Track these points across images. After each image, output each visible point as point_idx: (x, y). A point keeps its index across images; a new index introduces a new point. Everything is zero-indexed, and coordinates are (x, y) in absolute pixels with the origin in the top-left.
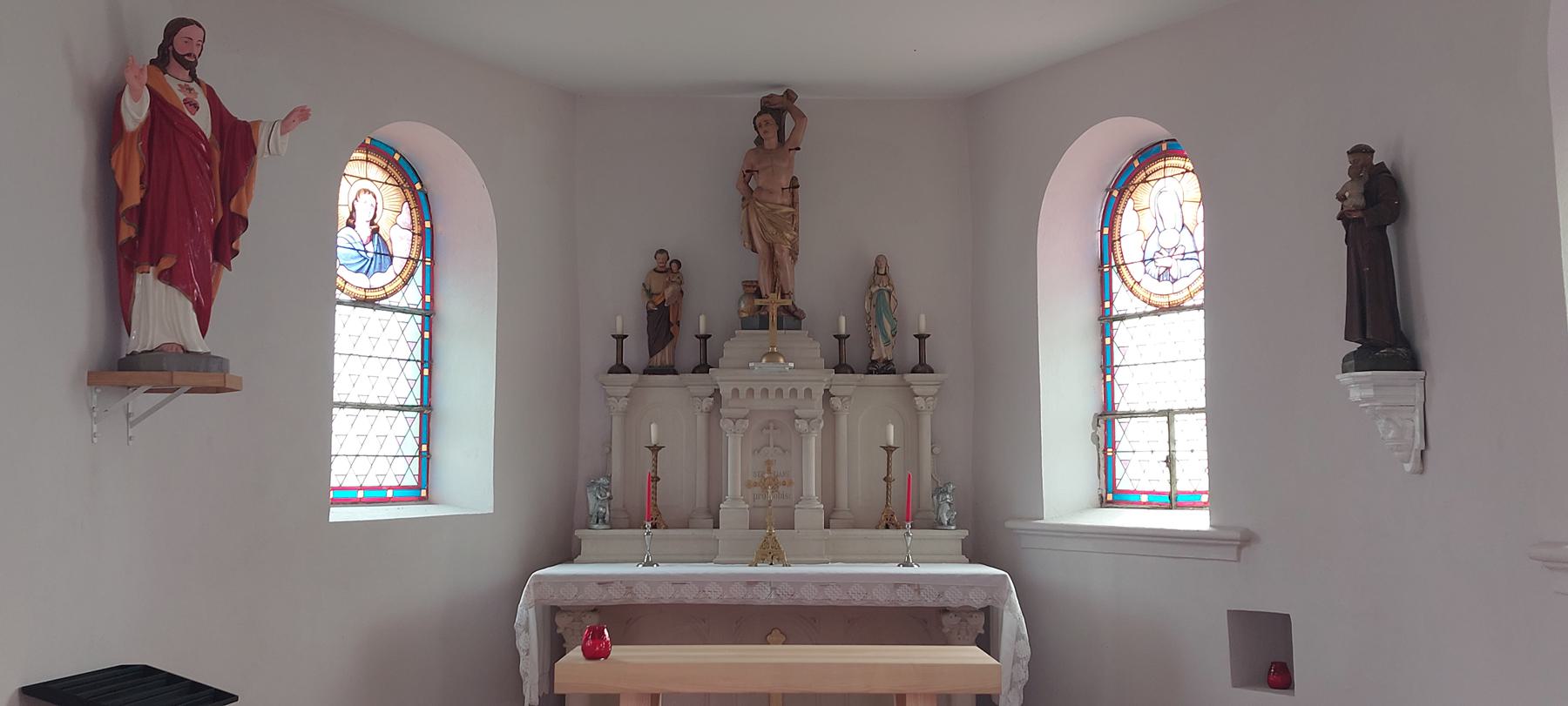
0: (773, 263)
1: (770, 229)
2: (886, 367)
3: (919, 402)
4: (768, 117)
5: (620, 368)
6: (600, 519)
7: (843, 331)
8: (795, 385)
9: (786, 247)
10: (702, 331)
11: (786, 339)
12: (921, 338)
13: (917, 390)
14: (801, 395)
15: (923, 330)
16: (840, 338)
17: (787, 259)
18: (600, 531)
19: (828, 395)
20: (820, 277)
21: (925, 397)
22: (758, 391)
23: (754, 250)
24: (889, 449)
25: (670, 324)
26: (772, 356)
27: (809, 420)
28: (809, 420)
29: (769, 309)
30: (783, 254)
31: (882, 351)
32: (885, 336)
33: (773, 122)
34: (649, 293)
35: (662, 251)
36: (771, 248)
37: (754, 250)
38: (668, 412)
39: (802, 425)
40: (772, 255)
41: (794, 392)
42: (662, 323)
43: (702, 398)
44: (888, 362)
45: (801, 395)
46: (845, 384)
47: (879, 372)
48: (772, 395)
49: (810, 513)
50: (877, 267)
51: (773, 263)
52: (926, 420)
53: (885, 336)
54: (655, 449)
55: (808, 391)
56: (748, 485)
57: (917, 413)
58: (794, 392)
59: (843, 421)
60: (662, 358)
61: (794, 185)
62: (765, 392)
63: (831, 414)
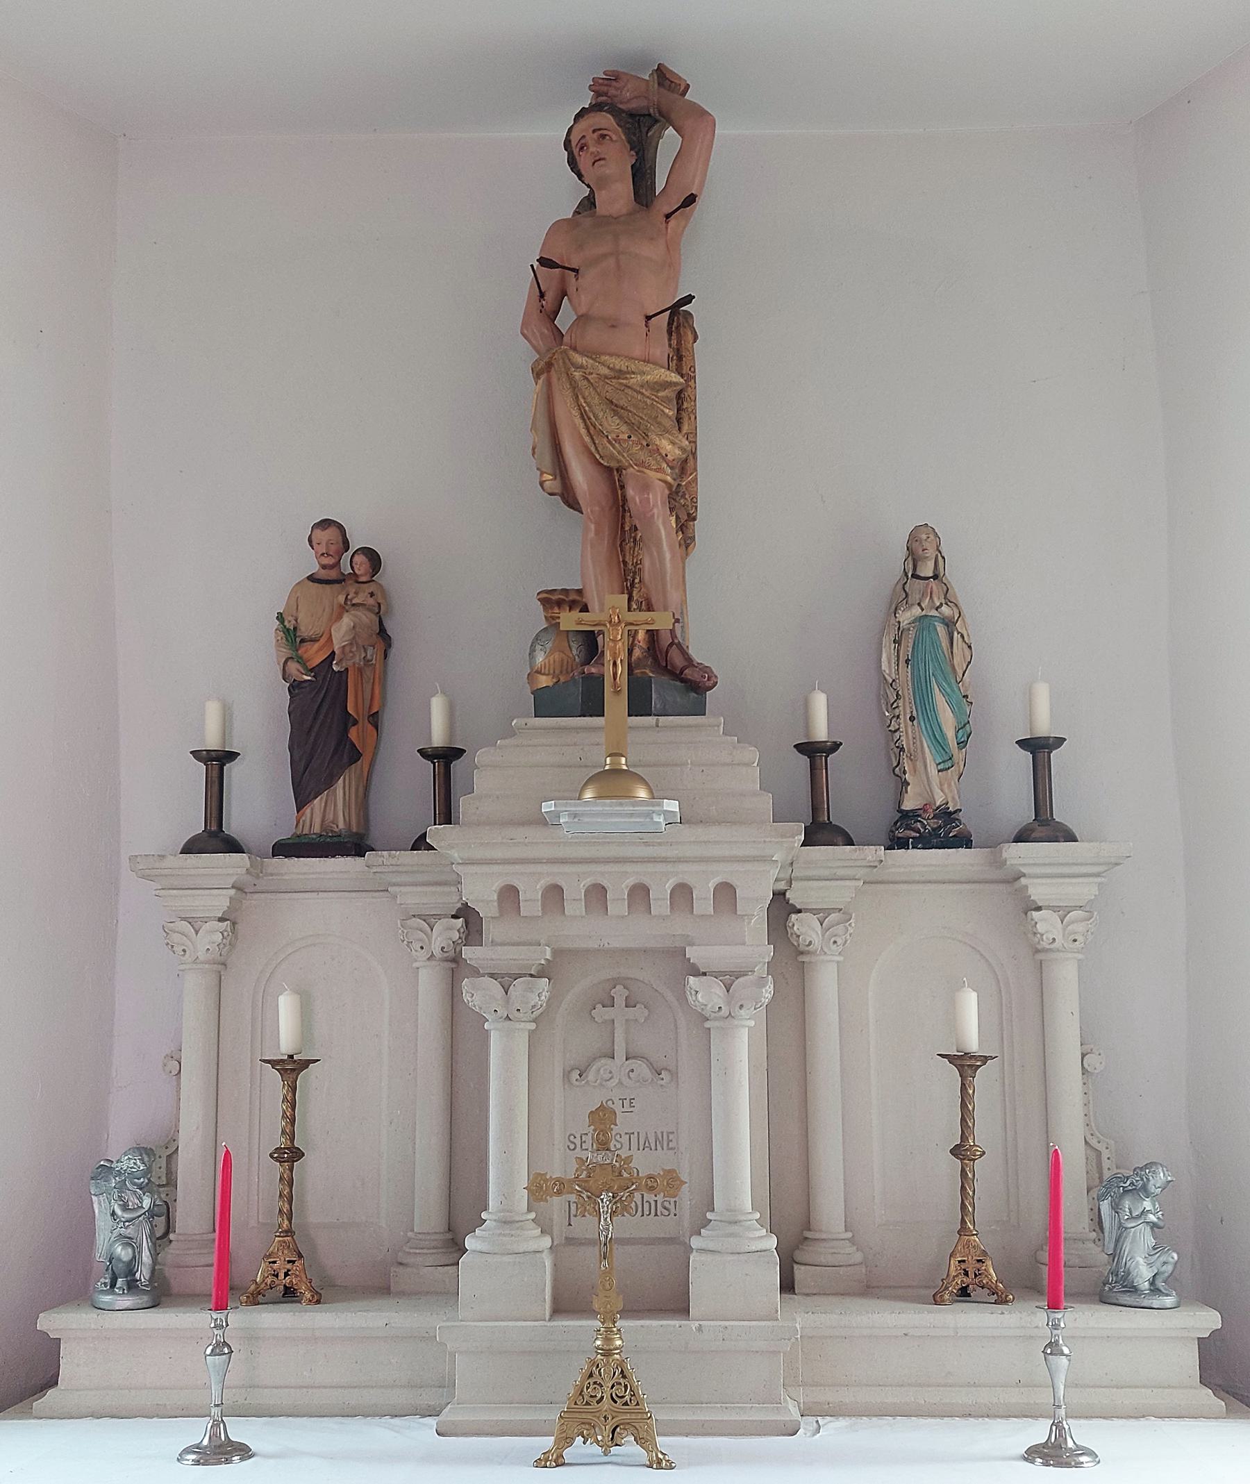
0: (623, 531)
1: (612, 425)
2: (942, 830)
3: (1046, 923)
4: (605, 120)
5: (215, 838)
6: (123, 1277)
7: (821, 733)
8: (687, 874)
9: (659, 479)
10: (438, 738)
11: (656, 739)
12: (1039, 748)
13: (1038, 891)
14: (704, 902)
15: (1044, 727)
16: (813, 751)
17: (664, 525)
18: (122, 1317)
19: (781, 907)
20: (760, 582)
21: (1063, 911)
22: (575, 891)
23: (569, 498)
24: (965, 1064)
25: (347, 721)
26: (613, 781)
27: (729, 978)
28: (729, 978)
29: (623, 669)
30: (649, 501)
31: (929, 787)
32: (939, 742)
33: (617, 134)
34: (291, 636)
35: (325, 524)
36: (613, 477)
37: (569, 498)
38: (341, 958)
39: (706, 994)
40: (619, 506)
41: (682, 893)
42: (331, 717)
43: (429, 920)
44: (948, 815)
45: (704, 902)
46: (833, 877)
47: (926, 841)
48: (618, 905)
49: (734, 1263)
50: (913, 556)
51: (623, 531)
52: (1066, 977)
53: (939, 742)
54: (291, 1068)
55: (726, 893)
56: (540, 1188)
57: (1038, 956)
58: (682, 893)
59: (826, 982)
60: (333, 809)
61: (678, 317)
62: (597, 894)
63: (792, 961)
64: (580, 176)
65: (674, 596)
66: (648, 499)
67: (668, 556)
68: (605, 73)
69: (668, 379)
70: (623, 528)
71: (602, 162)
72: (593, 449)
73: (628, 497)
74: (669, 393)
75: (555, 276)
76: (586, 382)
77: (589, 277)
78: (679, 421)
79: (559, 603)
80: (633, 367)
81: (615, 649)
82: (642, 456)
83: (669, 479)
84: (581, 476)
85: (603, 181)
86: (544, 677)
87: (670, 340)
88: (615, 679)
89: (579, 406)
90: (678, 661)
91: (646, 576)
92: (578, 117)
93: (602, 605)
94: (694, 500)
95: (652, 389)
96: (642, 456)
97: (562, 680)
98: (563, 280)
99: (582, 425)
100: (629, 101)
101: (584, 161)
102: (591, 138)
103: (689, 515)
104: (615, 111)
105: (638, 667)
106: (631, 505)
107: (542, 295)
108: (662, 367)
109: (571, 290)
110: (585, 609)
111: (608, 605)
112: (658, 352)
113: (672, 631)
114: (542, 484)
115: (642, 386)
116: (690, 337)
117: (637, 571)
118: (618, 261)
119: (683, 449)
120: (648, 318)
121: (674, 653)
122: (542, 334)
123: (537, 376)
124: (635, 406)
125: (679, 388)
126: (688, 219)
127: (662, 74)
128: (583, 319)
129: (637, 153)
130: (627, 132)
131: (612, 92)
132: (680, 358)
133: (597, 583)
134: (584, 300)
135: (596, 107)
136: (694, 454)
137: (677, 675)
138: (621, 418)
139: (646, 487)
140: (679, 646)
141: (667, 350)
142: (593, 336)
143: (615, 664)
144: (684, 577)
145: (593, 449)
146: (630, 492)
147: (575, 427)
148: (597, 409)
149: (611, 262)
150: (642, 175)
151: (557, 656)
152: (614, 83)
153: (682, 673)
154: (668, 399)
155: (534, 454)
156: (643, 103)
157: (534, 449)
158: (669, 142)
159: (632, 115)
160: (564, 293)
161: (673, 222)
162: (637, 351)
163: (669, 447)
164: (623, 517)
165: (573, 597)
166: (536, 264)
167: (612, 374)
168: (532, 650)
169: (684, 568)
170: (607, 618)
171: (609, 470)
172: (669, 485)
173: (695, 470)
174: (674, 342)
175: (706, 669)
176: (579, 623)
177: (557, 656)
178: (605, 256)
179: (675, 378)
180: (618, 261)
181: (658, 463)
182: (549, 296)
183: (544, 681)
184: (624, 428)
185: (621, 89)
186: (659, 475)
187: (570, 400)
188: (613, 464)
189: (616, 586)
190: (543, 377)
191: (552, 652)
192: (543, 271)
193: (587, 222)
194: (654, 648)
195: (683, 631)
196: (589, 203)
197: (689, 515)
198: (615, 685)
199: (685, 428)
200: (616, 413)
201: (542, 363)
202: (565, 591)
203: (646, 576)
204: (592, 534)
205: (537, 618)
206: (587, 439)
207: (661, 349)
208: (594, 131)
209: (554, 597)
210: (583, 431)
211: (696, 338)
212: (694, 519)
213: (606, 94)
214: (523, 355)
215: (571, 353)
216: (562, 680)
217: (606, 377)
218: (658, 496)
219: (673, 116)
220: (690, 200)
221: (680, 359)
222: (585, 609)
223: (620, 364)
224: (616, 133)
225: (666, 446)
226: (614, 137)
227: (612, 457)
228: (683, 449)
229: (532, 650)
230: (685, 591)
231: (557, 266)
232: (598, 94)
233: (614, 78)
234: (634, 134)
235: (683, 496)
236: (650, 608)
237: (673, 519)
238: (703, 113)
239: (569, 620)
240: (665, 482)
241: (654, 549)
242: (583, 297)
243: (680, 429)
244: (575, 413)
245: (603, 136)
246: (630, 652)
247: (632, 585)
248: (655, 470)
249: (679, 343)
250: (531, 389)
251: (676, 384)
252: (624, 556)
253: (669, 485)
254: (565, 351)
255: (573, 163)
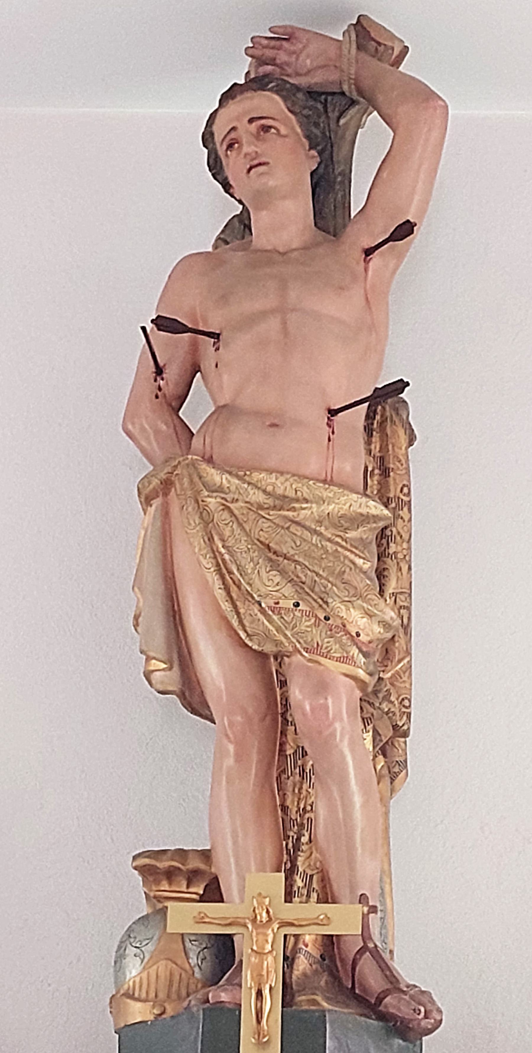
0: (282, 755)
1: (268, 584)
4: (270, 103)
17: (350, 746)
23: (193, 698)
30: (329, 709)
33: (288, 124)
36: (269, 670)
37: (193, 698)
40: (278, 715)
51: (282, 755)
64: (227, 187)
65: (367, 869)
66: (326, 708)
67: (357, 800)
68: (271, 30)
69: (364, 511)
70: (282, 750)
71: (261, 169)
72: (235, 623)
73: (292, 701)
74: (365, 533)
75: (180, 343)
76: (226, 515)
77: (237, 349)
78: (381, 575)
79: (170, 874)
80: (305, 492)
81: (261, 965)
82: (317, 636)
83: (361, 673)
84: (214, 664)
85: (264, 198)
86: (139, 1005)
87: (369, 443)
88: (259, 1021)
89: (215, 553)
90: (374, 981)
91: (321, 830)
92: (226, 97)
93: (242, 890)
94: (405, 704)
95: (335, 526)
96: (317, 636)
97: (170, 1011)
98: (194, 348)
99: (218, 584)
100: (308, 72)
101: (234, 166)
102: (246, 131)
103: (395, 727)
104: (286, 91)
105: (302, 991)
106: (296, 715)
107: (159, 371)
108: (357, 493)
109: (207, 364)
110: (213, 893)
111: (252, 886)
112: (348, 468)
113: (366, 934)
114: (148, 675)
115: (320, 522)
116: (403, 438)
117: (305, 823)
118: (284, 323)
119: (386, 625)
120: (333, 413)
121: (367, 965)
122: (157, 432)
123: (147, 501)
124: (307, 555)
125: (381, 524)
126: (400, 257)
127: (364, 32)
128: (224, 413)
129: (320, 153)
130: (307, 122)
131: (282, 57)
132: (385, 473)
133: (235, 843)
134: (228, 383)
135: (255, 83)
136: (406, 628)
137: (371, 1006)
138: (282, 572)
139: (322, 687)
140: (376, 954)
141: (362, 459)
142: (241, 441)
143: (259, 994)
144: (387, 829)
145: (235, 623)
146: (296, 693)
147: (206, 586)
148: (244, 560)
149: (274, 323)
150: (328, 186)
151: (163, 967)
152: (285, 44)
153: (380, 1000)
154: (363, 543)
155: (136, 625)
156: (334, 76)
157: (136, 618)
158: (371, 140)
159: (312, 94)
160: (196, 369)
161: (376, 258)
162: (314, 466)
163: (363, 622)
164: (284, 733)
165: (195, 863)
166: (150, 327)
167: (270, 502)
168: (120, 957)
169: (387, 814)
170: (251, 915)
171: (263, 656)
172: (362, 684)
173: (408, 653)
174: (376, 447)
175: (421, 998)
176: (201, 920)
177: (163, 967)
178: (264, 315)
179: (375, 508)
180: (284, 323)
181: (342, 646)
182: (172, 374)
183: (139, 1012)
184: (288, 590)
185: (297, 54)
186: (346, 668)
187: (199, 542)
188: (269, 648)
189: (270, 852)
190: (156, 503)
191: (154, 959)
192: (160, 338)
193: (236, 258)
194: (332, 959)
195: (383, 926)
196: (241, 225)
197: (395, 727)
198: (259, 1033)
199: (392, 586)
200: (274, 565)
201: (155, 482)
202: (182, 854)
203: (321, 830)
204: (230, 761)
205: (133, 899)
206: (226, 606)
207: (352, 460)
208: (251, 121)
209: (163, 864)
210: (220, 594)
211: (412, 440)
212: (405, 734)
213: (272, 62)
214: (130, 466)
215: (204, 466)
216: (170, 1011)
217: (260, 507)
218: (342, 703)
219: (380, 98)
220: (405, 230)
221: (384, 478)
222: (213, 893)
223: (283, 486)
224: (286, 122)
225: (356, 619)
226: (283, 131)
227: (267, 636)
228: (386, 625)
229: (120, 957)
230: (388, 854)
231: (185, 329)
232: (260, 61)
233: (285, 37)
234: (317, 125)
235: (387, 697)
236: (327, 897)
237: (369, 736)
238: (429, 96)
239: (186, 917)
240: (354, 678)
241: (334, 789)
242: (225, 377)
243: (381, 592)
244: (208, 563)
245: (266, 129)
246: (289, 961)
247: (297, 847)
248: (338, 660)
249: (384, 448)
250: (139, 522)
251: (376, 518)
252: (284, 797)
253: (362, 684)
254: (193, 464)
255: (216, 167)
